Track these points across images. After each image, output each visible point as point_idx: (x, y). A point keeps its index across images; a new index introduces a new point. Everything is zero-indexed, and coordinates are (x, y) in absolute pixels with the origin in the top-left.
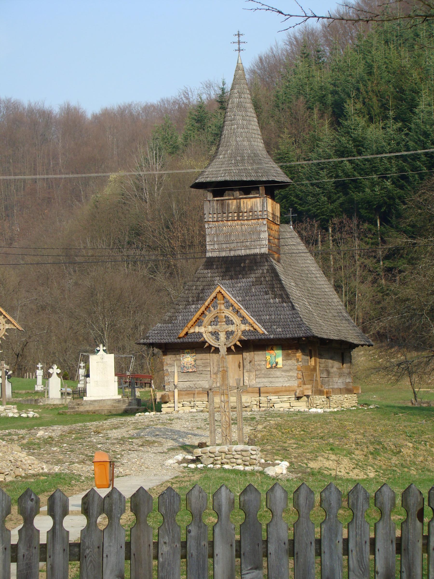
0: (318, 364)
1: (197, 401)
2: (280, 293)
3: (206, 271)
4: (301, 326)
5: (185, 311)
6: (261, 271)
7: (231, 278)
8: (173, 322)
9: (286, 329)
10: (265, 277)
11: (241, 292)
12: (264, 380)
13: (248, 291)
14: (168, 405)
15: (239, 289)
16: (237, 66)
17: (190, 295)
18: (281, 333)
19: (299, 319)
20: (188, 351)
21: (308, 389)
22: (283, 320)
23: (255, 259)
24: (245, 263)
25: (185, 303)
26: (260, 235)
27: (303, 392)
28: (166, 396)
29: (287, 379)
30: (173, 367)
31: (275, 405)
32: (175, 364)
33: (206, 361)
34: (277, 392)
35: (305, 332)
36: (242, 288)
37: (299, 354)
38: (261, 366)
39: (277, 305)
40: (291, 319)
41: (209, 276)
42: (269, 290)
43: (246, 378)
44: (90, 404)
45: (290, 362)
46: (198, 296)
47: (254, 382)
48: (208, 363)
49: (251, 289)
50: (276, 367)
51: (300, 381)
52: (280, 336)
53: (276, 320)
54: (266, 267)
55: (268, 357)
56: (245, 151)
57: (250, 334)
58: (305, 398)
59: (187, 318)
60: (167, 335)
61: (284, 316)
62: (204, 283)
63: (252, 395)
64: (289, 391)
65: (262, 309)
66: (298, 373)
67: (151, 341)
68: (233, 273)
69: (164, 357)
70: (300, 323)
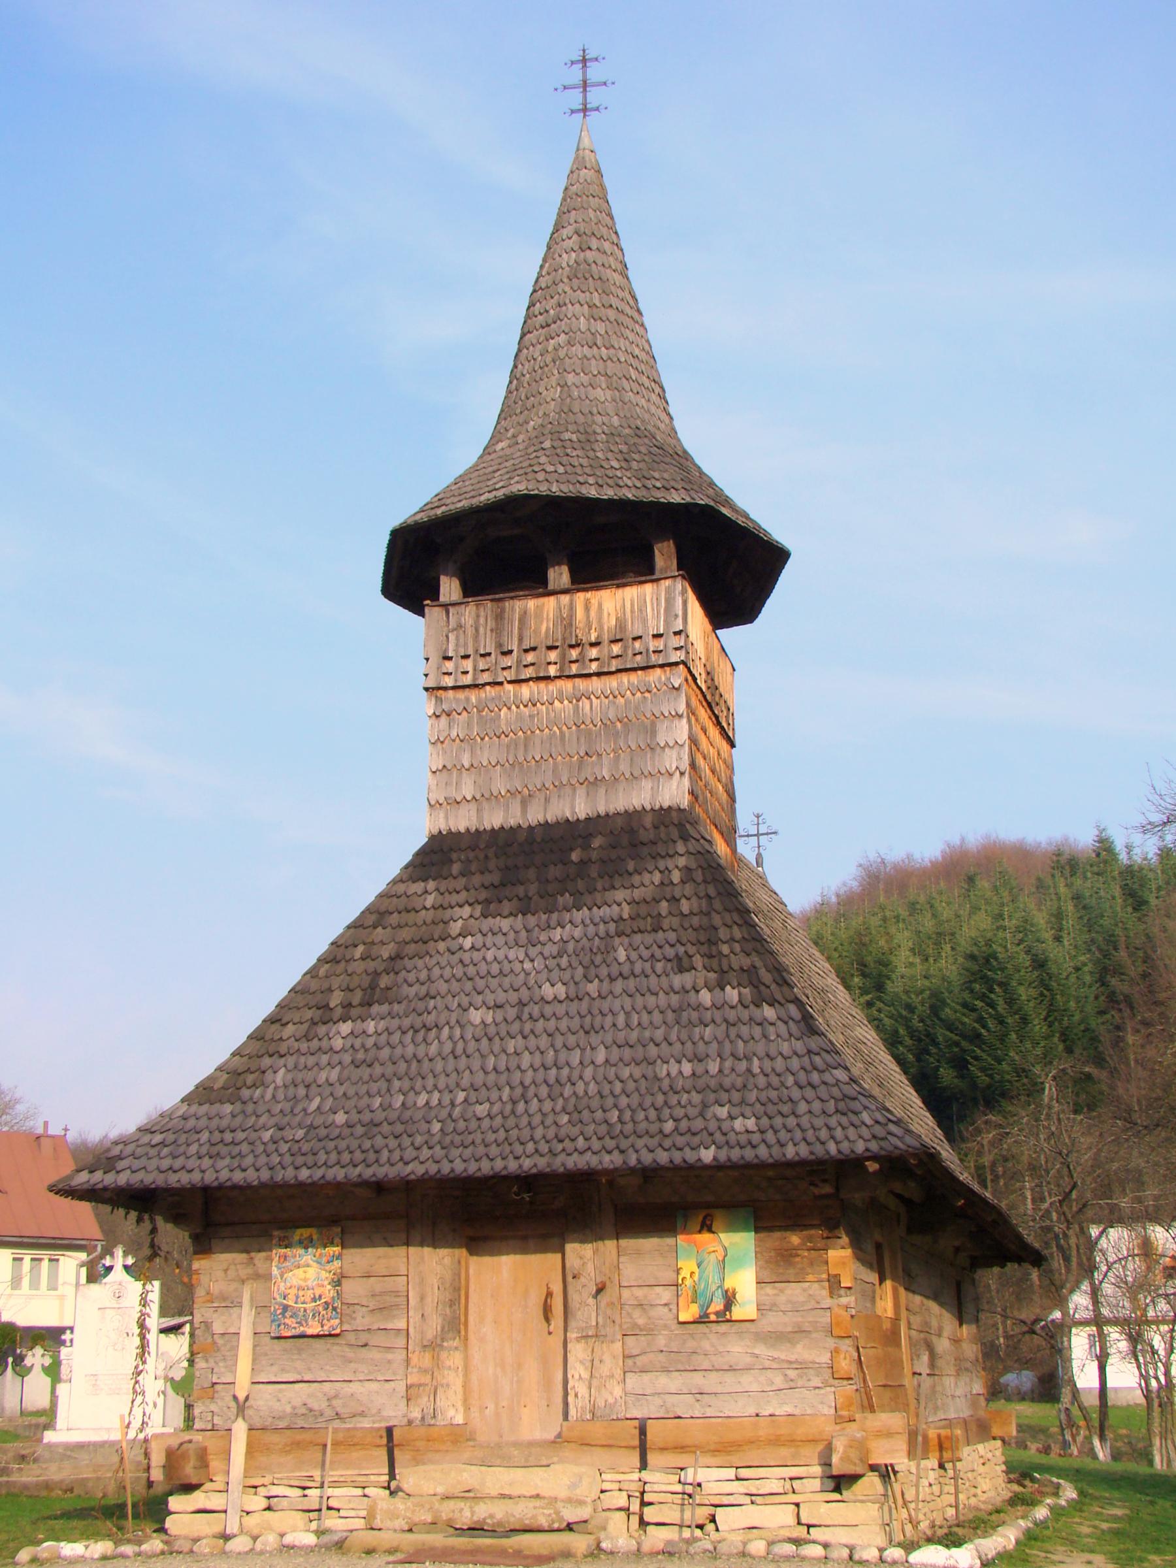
0: (904, 1314)
1: (336, 1484)
2: (746, 962)
3: (418, 887)
4: (856, 1105)
5: (304, 1046)
6: (657, 877)
7: (525, 910)
8: (245, 1093)
9: (778, 1121)
10: (674, 900)
11: (564, 962)
12: (665, 1382)
13: (598, 959)
14: (198, 1499)
15: (554, 949)
16: (577, 158)
17: (336, 982)
18: (756, 1138)
19: (840, 1074)
20: (304, 1232)
22: (762, 1081)
23: (632, 831)
24: (586, 847)
25: (309, 1014)
26: (654, 733)
27: (862, 1447)
28: (184, 1456)
29: (779, 1381)
31: (720, 1514)
34: (727, 1447)
35: (878, 1130)
36: (571, 946)
37: (840, 1255)
39: (732, 1015)
40: (802, 1076)
41: (428, 904)
42: (692, 950)
43: (577, 1370)
44: (64, 1457)
45: (794, 1292)
46: (373, 987)
47: (618, 1391)
48: (396, 1293)
49: (609, 949)
50: (724, 1316)
51: (849, 1388)
52: (749, 1154)
53: (727, 1082)
54: (682, 862)
55: (688, 1266)
56: (598, 419)
57: (596, 1145)
58: (871, 1483)
59: (309, 1076)
60: (204, 1150)
61: (767, 1065)
62: (405, 934)
63: (603, 1457)
64: (792, 1442)
65: (659, 1034)
66: (836, 1351)
67: (123, 1179)
68: (533, 889)
69: (196, 1265)
70: (848, 1090)
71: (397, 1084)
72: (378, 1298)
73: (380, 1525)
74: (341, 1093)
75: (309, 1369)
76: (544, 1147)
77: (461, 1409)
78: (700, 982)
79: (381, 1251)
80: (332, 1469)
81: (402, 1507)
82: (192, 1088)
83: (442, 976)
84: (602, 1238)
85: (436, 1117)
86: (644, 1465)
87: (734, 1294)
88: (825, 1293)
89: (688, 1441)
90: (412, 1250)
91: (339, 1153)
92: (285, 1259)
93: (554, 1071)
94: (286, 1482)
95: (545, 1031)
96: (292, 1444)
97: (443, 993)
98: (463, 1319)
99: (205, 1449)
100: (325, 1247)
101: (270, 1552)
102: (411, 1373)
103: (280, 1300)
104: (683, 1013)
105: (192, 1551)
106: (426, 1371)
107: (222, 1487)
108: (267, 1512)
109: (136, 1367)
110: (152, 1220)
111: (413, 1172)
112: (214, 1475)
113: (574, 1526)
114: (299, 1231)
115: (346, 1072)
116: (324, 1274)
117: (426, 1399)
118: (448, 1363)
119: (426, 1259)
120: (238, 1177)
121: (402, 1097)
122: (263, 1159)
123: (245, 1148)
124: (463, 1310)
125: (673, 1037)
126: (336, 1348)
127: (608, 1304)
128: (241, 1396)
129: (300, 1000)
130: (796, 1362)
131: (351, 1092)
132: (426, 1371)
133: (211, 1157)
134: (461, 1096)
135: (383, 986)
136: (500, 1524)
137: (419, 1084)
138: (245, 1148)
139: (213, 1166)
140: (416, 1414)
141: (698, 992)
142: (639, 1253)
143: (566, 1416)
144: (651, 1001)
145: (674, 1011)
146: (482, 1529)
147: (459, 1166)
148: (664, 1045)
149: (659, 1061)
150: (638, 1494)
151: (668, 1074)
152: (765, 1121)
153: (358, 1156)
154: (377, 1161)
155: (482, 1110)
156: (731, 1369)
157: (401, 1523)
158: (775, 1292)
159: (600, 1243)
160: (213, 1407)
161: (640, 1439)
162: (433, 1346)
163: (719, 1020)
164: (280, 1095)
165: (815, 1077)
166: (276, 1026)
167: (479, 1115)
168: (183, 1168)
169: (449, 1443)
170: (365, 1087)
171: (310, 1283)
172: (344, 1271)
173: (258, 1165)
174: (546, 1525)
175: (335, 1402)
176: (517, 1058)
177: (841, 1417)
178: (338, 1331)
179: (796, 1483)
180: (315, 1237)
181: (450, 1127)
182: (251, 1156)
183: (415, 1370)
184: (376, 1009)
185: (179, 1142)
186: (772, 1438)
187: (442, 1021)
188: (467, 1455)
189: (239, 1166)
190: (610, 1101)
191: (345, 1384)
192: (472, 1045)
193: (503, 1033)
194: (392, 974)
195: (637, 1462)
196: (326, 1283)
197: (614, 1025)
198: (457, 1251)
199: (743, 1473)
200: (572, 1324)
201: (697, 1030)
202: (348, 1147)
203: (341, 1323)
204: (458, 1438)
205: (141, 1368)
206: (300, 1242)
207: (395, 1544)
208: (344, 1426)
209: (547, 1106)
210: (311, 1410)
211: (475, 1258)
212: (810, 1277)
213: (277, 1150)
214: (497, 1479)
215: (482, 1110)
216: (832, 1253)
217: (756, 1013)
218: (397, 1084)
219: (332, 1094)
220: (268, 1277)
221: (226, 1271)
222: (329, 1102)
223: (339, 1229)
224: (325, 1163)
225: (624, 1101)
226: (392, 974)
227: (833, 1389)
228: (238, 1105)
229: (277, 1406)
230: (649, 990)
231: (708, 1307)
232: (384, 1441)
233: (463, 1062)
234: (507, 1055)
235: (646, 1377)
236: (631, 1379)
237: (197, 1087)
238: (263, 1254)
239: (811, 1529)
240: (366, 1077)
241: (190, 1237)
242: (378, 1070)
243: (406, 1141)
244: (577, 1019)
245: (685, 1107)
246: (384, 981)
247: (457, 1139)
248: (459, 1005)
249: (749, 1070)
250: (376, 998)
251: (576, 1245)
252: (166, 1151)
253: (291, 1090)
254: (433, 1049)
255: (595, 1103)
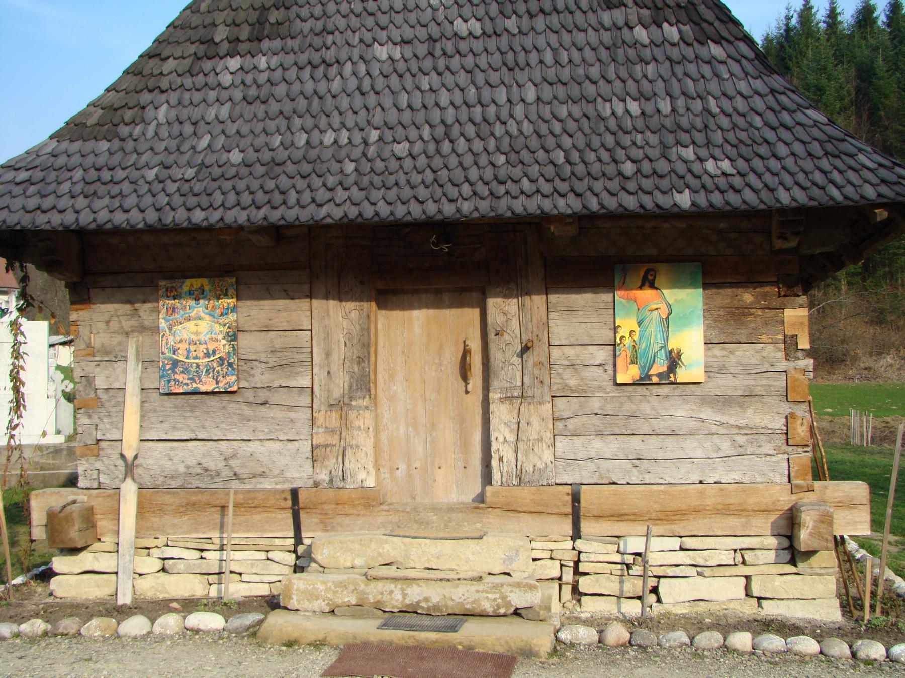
1: (237, 547)
5: (188, 82)
9: (757, 163)
12: (597, 446)
14: (86, 560)
18: (737, 181)
20: (196, 283)
21: (849, 505)
22: (725, 122)
25: (192, 49)
28: (69, 519)
29: (726, 447)
30: (119, 366)
32: (131, 352)
33: (291, 339)
34: (668, 516)
38: (587, 373)
40: (770, 116)
43: (501, 433)
45: (746, 353)
47: (547, 456)
48: (299, 349)
50: (668, 377)
55: (627, 324)
59: (196, 113)
60: (78, 189)
61: (726, 105)
64: (741, 511)
66: (789, 419)
69: (74, 316)
71: (297, 122)
72: (278, 354)
73: (297, 606)
74: (234, 131)
75: (203, 427)
76: (484, 190)
77: (372, 471)
78: (633, 19)
79: (281, 303)
80: (233, 531)
81: (321, 587)
82: (63, 125)
83: (338, 11)
84: (529, 293)
85: (348, 156)
86: (576, 535)
87: (679, 355)
88: (781, 355)
89: (626, 509)
90: (316, 303)
91: (238, 194)
92: (174, 311)
93: (478, 110)
94: (181, 544)
95: (463, 68)
96: (187, 504)
97: (342, 29)
98: (372, 376)
99: (91, 510)
100: (218, 298)
101: (172, 637)
102: (317, 433)
103: (169, 354)
104: (616, 47)
105: (79, 634)
106: (333, 431)
107: (111, 548)
108: (161, 574)
109: (10, 422)
110: (22, 268)
111: (329, 216)
112: (101, 535)
113: (523, 612)
114: (188, 282)
115: (237, 110)
116: (218, 328)
117: (334, 460)
118: (357, 423)
119: (331, 312)
120: (119, 219)
121: (305, 136)
122: (148, 200)
123: (126, 187)
124: (372, 367)
125: (612, 75)
126: (233, 406)
127: (535, 365)
128: (129, 455)
129: (180, 35)
130: (746, 427)
131: (245, 130)
132: (333, 431)
133: (86, 197)
134: (374, 135)
135: (273, 20)
136: (436, 607)
137: (323, 122)
138: (126, 187)
139: (89, 207)
140: (323, 476)
141: (631, 28)
142: (570, 309)
143: (487, 478)
144: (580, 38)
145: (608, 48)
146: (416, 612)
147: (384, 211)
148: (602, 83)
149: (599, 100)
150: (572, 564)
151: (613, 114)
152: (740, 163)
153: (261, 197)
154: (284, 203)
155: (401, 149)
156: (673, 434)
157: (321, 605)
158: (725, 353)
159: (527, 298)
160: (98, 465)
161: (573, 506)
162: (341, 406)
163: (660, 58)
164: (164, 133)
165: (786, 117)
166: (153, 62)
167: (399, 154)
168: (54, 207)
169: (360, 507)
170: (261, 126)
171: (202, 337)
172: (240, 326)
173: (142, 207)
174: (490, 610)
175: (232, 462)
176: (434, 95)
177: (798, 486)
178: (235, 388)
179: (748, 556)
180: (206, 288)
181: (367, 167)
182: (134, 195)
183: (321, 430)
184: (266, 44)
185: (48, 181)
186: (720, 507)
187: (343, 56)
188: (380, 520)
189: (121, 207)
190: (550, 142)
191: (244, 444)
192: (380, 83)
193: (415, 70)
194: (282, 9)
195: (568, 529)
196: (220, 337)
197: (541, 62)
198: (365, 305)
199: (689, 543)
200: (495, 384)
201: (638, 68)
202: (248, 188)
203: (238, 379)
204: (369, 501)
205: (16, 422)
206: (190, 293)
207: (321, 636)
208: (243, 486)
209: (478, 145)
210: (206, 470)
211: (383, 312)
212: (764, 338)
213: (164, 190)
214: (422, 553)
215: (401, 149)
216: (788, 313)
217: (703, 51)
218: (297, 122)
219: (223, 132)
220: (155, 330)
221: (107, 323)
222: (221, 141)
223: (234, 280)
224: (223, 205)
225: (567, 141)
226: (282, 9)
227: (786, 456)
228: (116, 143)
229: (168, 465)
230: (576, 26)
231: (649, 369)
232: (289, 503)
233: (372, 100)
234: (421, 91)
235: (578, 441)
236: (561, 443)
237: (67, 123)
238: (148, 306)
239: (764, 603)
240: (261, 114)
241: (67, 286)
242: (274, 107)
243: (317, 182)
244: (497, 56)
245: (642, 147)
246: (274, 16)
247: (377, 180)
248: (361, 41)
249: (706, 110)
250: (266, 32)
251: (499, 300)
252: (32, 189)
253: (176, 128)
254: (336, 85)
255: (534, 143)
